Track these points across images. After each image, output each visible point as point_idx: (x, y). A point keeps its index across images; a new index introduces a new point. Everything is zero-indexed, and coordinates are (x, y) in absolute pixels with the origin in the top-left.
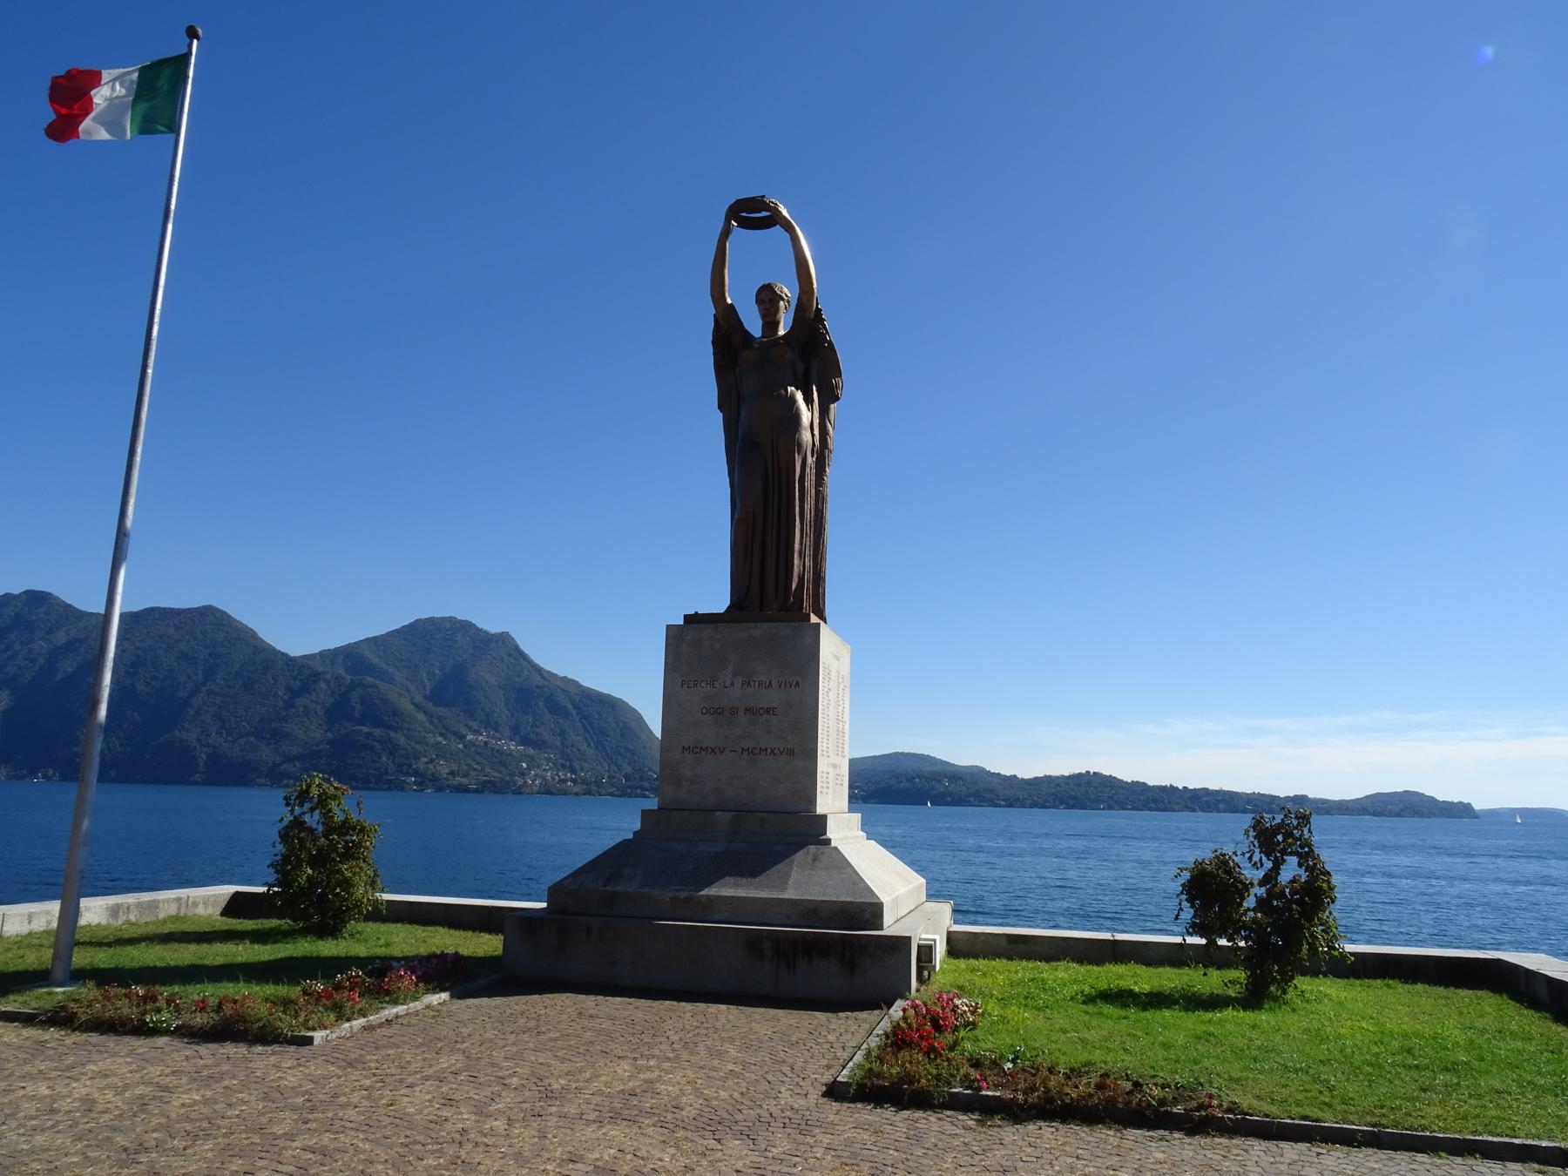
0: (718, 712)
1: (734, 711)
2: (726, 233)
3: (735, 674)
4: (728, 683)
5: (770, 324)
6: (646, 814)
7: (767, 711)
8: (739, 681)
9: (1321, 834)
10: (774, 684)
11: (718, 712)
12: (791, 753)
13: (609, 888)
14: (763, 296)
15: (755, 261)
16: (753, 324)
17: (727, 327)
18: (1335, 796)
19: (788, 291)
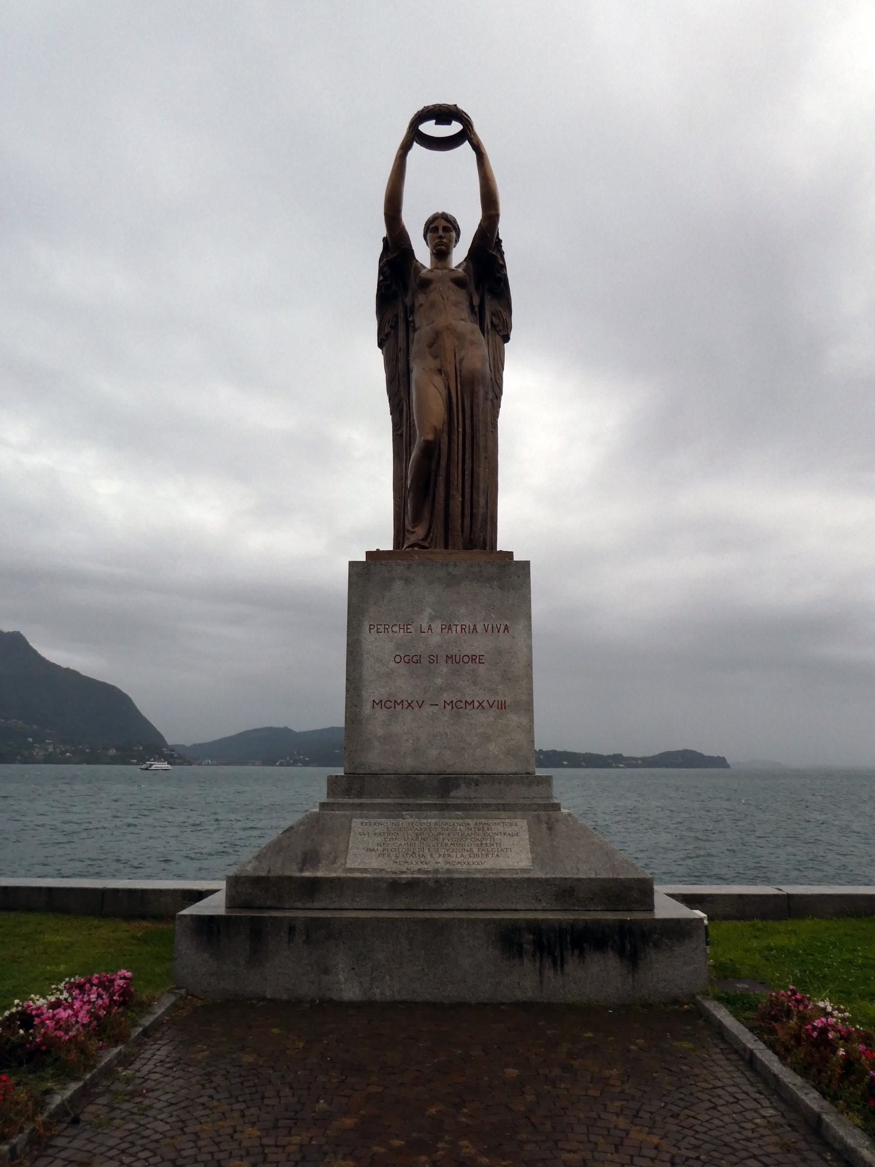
0: (412, 660)
1: (433, 659)
2: (405, 148)
3: (432, 618)
4: (425, 627)
5: (441, 253)
6: (333, 781)
7: (473, 658)
8: (437, 626)
9: (569, 791)
10: (480, 628)
11: (412, 660)
12: (502, 706)
13: (306, 874)
14: (444, 223)
15: (442, 185)
16: (423, 254)
17: (396, 248)
18: (639, 755)
19: (469, 222)
